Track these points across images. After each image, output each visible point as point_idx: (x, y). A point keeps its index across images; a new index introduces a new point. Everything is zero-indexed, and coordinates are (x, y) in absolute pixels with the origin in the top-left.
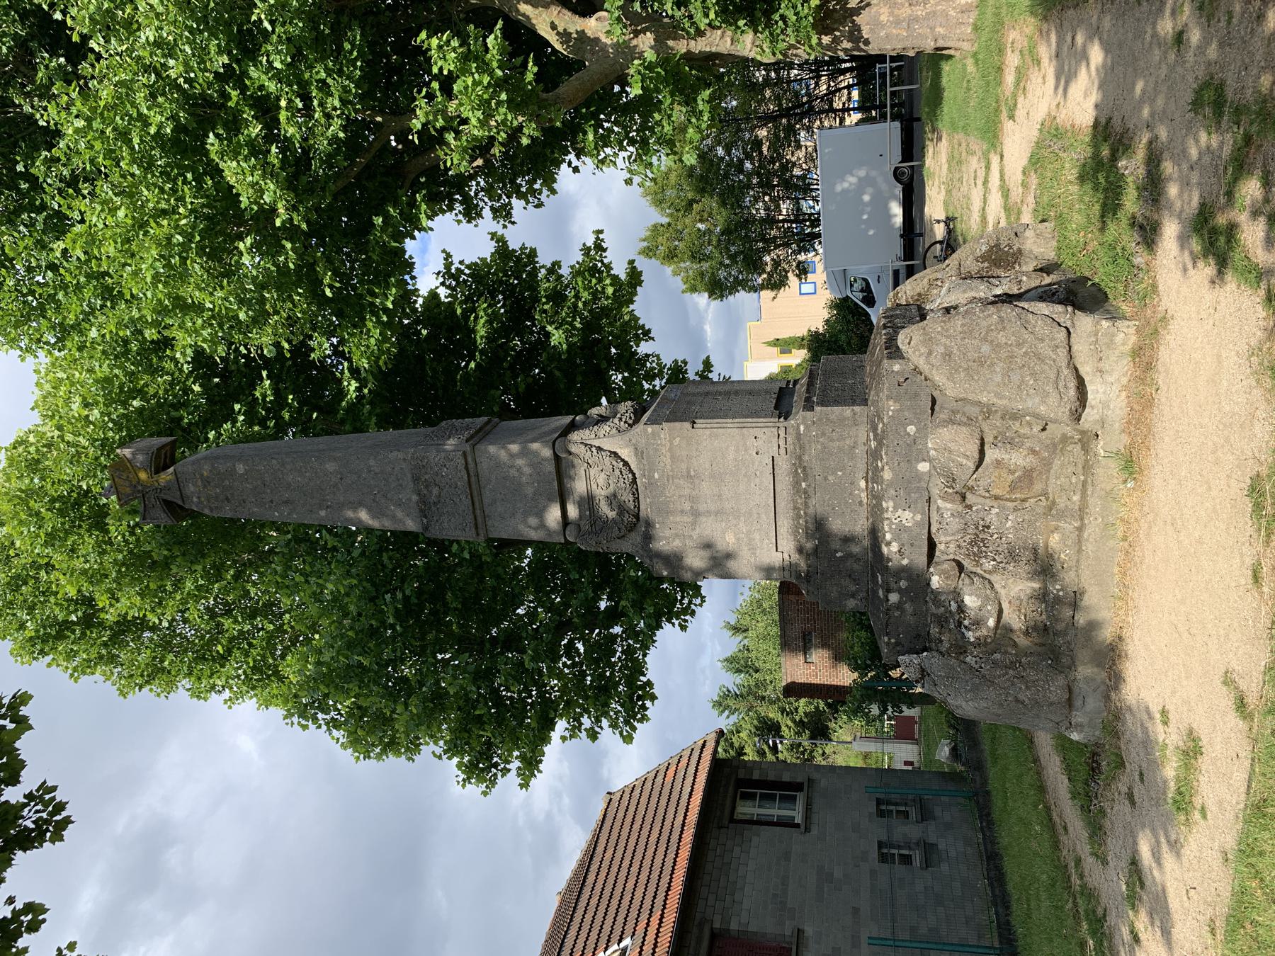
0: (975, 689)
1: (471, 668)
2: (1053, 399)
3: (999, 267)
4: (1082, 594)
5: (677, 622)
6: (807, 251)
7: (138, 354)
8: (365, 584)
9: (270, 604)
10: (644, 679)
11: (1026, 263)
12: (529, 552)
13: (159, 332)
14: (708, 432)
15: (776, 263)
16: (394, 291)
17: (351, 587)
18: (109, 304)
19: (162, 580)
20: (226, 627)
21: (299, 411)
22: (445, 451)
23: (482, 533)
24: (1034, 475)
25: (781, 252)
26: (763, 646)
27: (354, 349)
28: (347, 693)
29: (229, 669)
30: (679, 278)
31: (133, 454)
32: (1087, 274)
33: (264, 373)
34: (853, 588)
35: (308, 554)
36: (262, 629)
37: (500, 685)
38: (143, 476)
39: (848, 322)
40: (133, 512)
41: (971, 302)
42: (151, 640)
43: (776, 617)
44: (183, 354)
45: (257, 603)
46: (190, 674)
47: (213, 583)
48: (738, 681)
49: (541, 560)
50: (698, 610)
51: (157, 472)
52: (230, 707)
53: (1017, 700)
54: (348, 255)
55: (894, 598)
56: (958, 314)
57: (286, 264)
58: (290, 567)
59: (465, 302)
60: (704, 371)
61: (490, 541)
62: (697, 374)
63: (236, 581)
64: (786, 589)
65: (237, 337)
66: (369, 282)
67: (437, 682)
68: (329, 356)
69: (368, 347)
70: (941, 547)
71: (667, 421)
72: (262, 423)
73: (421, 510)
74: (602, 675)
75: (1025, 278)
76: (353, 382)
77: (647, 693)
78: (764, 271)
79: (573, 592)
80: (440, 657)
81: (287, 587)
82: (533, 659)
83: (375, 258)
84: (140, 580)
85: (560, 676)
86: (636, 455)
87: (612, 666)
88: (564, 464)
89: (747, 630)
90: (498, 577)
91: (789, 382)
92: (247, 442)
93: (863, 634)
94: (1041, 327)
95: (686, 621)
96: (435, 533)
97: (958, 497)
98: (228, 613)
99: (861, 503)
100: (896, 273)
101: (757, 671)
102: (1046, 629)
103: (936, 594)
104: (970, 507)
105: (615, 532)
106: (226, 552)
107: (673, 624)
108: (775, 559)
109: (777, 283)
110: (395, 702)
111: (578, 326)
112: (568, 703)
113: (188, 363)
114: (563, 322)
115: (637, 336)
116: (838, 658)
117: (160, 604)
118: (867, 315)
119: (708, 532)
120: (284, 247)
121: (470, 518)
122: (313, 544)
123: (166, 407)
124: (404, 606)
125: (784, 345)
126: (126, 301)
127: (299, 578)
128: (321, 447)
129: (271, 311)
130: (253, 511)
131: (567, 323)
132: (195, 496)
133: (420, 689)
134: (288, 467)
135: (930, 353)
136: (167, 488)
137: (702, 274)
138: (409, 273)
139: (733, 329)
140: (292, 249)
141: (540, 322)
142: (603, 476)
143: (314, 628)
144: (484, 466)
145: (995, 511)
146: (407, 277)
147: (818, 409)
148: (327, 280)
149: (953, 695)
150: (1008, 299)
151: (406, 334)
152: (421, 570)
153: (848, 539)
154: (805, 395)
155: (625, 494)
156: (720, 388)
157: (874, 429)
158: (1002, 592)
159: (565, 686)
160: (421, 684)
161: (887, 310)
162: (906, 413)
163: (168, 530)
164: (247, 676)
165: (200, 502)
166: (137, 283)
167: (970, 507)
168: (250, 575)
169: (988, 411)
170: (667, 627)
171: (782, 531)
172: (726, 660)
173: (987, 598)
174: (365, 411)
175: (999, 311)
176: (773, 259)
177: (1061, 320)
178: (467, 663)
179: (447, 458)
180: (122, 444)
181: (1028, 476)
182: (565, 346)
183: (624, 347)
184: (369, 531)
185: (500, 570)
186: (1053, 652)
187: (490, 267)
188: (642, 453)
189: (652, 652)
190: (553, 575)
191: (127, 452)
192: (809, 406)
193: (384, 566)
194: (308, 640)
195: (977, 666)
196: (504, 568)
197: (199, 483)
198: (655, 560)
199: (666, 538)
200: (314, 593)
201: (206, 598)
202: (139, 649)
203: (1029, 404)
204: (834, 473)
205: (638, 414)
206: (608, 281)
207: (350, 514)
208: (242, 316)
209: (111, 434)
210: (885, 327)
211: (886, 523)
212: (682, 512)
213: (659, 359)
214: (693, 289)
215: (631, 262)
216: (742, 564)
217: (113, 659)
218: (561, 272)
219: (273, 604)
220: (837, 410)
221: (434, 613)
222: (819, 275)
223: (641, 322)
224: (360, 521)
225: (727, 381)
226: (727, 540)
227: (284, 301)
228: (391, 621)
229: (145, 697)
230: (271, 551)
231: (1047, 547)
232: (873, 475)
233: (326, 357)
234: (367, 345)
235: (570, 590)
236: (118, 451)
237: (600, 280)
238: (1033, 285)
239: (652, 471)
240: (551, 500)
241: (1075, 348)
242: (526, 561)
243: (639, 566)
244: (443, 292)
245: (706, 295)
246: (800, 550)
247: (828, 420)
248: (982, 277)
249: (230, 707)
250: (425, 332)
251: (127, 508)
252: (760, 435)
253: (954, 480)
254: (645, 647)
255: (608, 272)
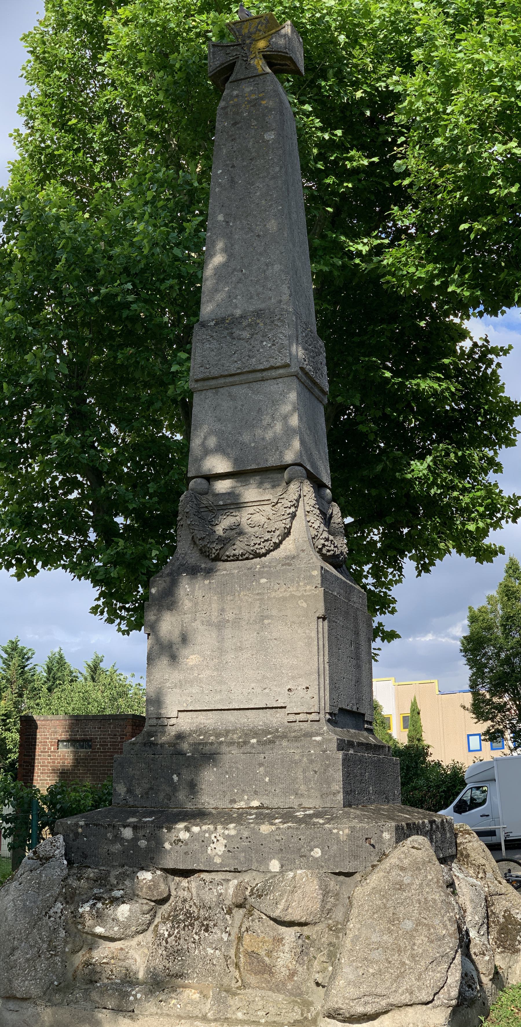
0: (27, 910)
1: (52, 377)
2: (353, 992)
3: (499, 933)
4: (131, 1018)
5: (100, 603)
6: (514, 739)
7: (396, 42)
8: (143, 262)
9: (121, 167)
10: (39, 566)
11: (504, 958)
12: (179, 437)
13: (420, 62)
14: (314, 634)
15: (501, 708)
16: (467, 294)
17: (140, 248)
18: (449, 20)
19: (147, 64)
20: (96, 126)
21: (334, 193)
22: (290, 345)
23: (198, 385)
24: (266, 976)
25: (514, 711)
26: (76, 697)
27: (403, 250)
28: (26, 249)
29: (51, 131)
30: (484, 603)
31: (285, 36)
32: (492, 1015)
33: (376, 159)
34: (138, 792)
35: (177, 204)
36: (95, 161)
37: (33, 409)
38: (262, 44)
39: (438, 787)
40: (222, 35)
41: (460, 908)
42: (83, 57)
43: (108, 712)
44: (395, 82)
45: (124, 155)
46: (46, 95)
47: (144, 111)
48: (39, 669)
49: (169, 449)
50: (114, 627)
51: (265, 57)
52: (11, 135)
53: (14, 949)
54: (505, 248)
55: (128, 833)
56: (447, 895)
57: (495, 186)
58: (162, 186)
59: (456, 368)
60: (383, 632)
61: (190, 394)
62: (380, 624)
63: (146, 134)
64: (138, 722)
65: (415, 135)
66: (476, 269)
67: (37, 342)
68: (395, 225)
69: (406, 265)
70: (184, 883)
71: (325, 593)
72: (321, 157)
73: (223, 319)
74: (43, 520)
75: (487, 958)
76: (367, 248)
77: (25, 569)
78: (493, 695)
79: (134, 486)
80: (64, 343)
81: (140, 184)
82: (60, 444)
83: (502, 276)
84: (148, 43)
85: (43, 474)
86: (287, 558)
87: (53, 531)
88: (277, 476)
89: (93, 679)
90: (150, 403)
91: (370, 723)
92: (300, 142)
93: (90, 802)
94: (433, 977)
95: (102, 613)
96: (198, 334)
97: (240, 900)
98: (112, 127)
99: (233, 801)
100: (492, 833)
101: (50, 690)
102: (92, 982)
103: (133, 876)
104: (229, 912)
105: (200, 534)
106: (178, 122)
107: (98, 599)
108: (171, 709)
109: (479, 709)
110: (17, 299)
111: (432, 492)
112: (13, 483)
113: (387, 87)
114: (436, 475)
115: (423, 557)
116: (64, 775)
117: (122, 63)
118: (446, 806)
119: (199, 639)
120: (512, 185)
121: (215, 372)
122: (187, 208)
123: (338, 65)
124: (119, 304)
125: (412, 721)
126: (454, 35)
127: (149, 195)
128: (294, 215)
129: (444, 169)
130: (223, 147)
131: (435, 479)
132: (237, 93)
133: (30, 325)
134: (271, 183)
135: (402, 869)
136: (248, 66)
137: (489, 628)
138: (486, 310)
139: (431, 665)
140: (510, 193)
141: (436, 449)
142: (264, 520)
143: (96, 212)
144: (273, 387)
145: (225, 937)
146: (482, 308)
147: (340, 755)
148: (477, 226)
149: (21, 887)
150: (464, 944)
151: (420, 305)
152: (158, 320)
153: (193, 788)
154: (355, 741)
155: (242, 545)
156: (363, 648)
157: (318, 815)
158: (133, 942)
159: (33, 479)
160: (35, 325)
161: (450, 824)
162: (335, 847)
163: (202, 68)
164: (43, 149)
165: (232, 98)
166: (473, 46)
167: (229, 912)
168: (153, 147)
169: (338, 929)
170: (95, 592)
171: (202, 716)
172: (61, 658)
173: (126, 926)
174: (335, 260)
175: (450, 935)
176: (505, 703)
177: (441, 995)
178: (58, 373)
179: (282, 346)
180: (295, 25)
181: (266, 970)
182: (409, 476)
183: (410, 543)
184: (201, 265)
185: (158, 405)
186: (67, 987)
187: (495, 395)
188: (289, 565)
189: (68, 575)
190: (153, 464)
191: (288, 29)
192: (342, 745)
193: (162, 281)
194: (83, 207)
195: (51, 912)
196: (161, 409)
197: (253, 97)
198: (168, 579)
199: (193, 592)
200: (133, 211)
201: (128, 105)
202: (73, 46)
203: (346, 970)
204: (266, 774)
205: (333, 560)
206: (481, 525)
207: (220, 245)
208: (438, 141)
209: (308, 15)
210: (432, 822)
211: (211, 827)
212: (223, 610)
213: (397, 582)
214: (473, 619)
215: (502, 550)
216: (165, 673)
217: (61, 25)
218: (491, 472)
219: (121, 170)
220: (339, 776)
221: (112, 335)
222: (488, 753)
223: (437, 562)
224: (212, 256)
225: (372, 657)
226: (191, 658)
227: (454, 182)
228: (103, 291)
229: (23, 57)
230: (180, 167)
231: (185, 987)
232: (264, 814)
233: (394, 221)
234: (407, 265)
235: (137, 482)
236: (289, 22)
237: (482, 516)
238: (480, 967)
239: (269, 576)
240: (236, 461)
241: (410, 1010)
242: (168, 434)
243: (163, 561)
244: (467, 344)
245: (467, 634)
246: (180, 736)
247: (328, 766)
248: (488, 917)
249: (11, 135)
250: (423, 324)
251: (226, 30)
252: (311, 692)
253: (260, 896)
254: (72, 567)
255: (491, 525)
